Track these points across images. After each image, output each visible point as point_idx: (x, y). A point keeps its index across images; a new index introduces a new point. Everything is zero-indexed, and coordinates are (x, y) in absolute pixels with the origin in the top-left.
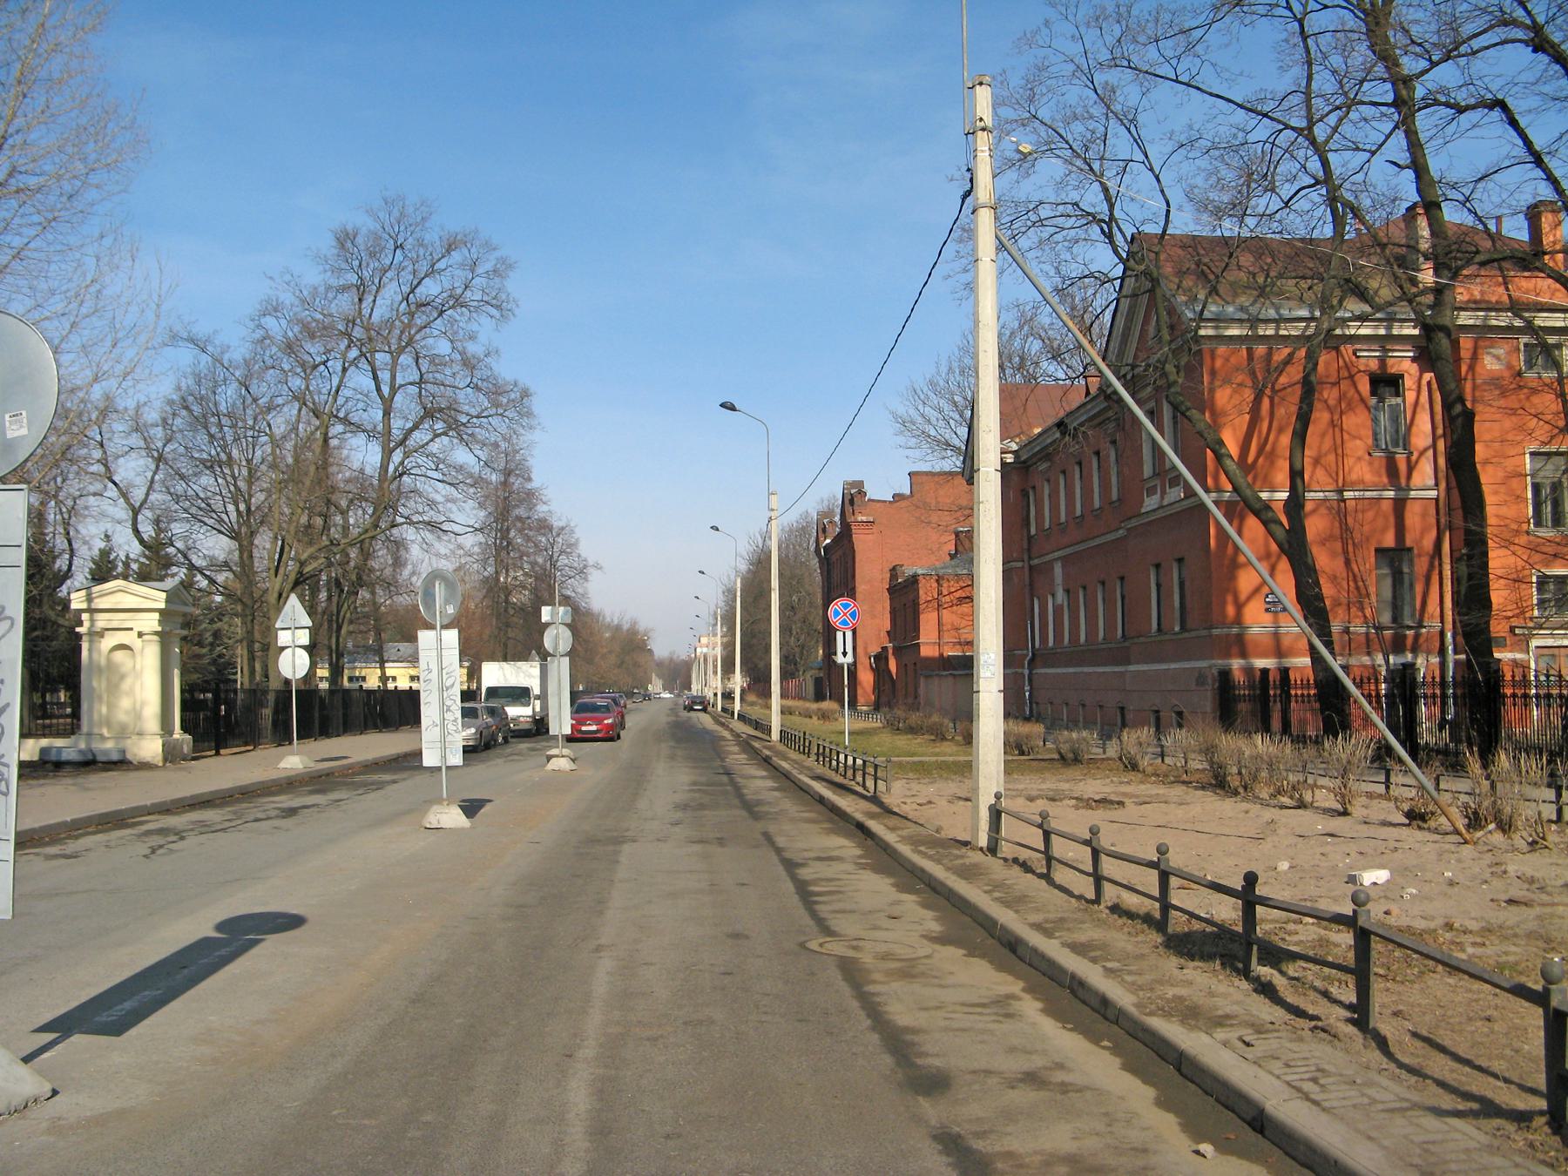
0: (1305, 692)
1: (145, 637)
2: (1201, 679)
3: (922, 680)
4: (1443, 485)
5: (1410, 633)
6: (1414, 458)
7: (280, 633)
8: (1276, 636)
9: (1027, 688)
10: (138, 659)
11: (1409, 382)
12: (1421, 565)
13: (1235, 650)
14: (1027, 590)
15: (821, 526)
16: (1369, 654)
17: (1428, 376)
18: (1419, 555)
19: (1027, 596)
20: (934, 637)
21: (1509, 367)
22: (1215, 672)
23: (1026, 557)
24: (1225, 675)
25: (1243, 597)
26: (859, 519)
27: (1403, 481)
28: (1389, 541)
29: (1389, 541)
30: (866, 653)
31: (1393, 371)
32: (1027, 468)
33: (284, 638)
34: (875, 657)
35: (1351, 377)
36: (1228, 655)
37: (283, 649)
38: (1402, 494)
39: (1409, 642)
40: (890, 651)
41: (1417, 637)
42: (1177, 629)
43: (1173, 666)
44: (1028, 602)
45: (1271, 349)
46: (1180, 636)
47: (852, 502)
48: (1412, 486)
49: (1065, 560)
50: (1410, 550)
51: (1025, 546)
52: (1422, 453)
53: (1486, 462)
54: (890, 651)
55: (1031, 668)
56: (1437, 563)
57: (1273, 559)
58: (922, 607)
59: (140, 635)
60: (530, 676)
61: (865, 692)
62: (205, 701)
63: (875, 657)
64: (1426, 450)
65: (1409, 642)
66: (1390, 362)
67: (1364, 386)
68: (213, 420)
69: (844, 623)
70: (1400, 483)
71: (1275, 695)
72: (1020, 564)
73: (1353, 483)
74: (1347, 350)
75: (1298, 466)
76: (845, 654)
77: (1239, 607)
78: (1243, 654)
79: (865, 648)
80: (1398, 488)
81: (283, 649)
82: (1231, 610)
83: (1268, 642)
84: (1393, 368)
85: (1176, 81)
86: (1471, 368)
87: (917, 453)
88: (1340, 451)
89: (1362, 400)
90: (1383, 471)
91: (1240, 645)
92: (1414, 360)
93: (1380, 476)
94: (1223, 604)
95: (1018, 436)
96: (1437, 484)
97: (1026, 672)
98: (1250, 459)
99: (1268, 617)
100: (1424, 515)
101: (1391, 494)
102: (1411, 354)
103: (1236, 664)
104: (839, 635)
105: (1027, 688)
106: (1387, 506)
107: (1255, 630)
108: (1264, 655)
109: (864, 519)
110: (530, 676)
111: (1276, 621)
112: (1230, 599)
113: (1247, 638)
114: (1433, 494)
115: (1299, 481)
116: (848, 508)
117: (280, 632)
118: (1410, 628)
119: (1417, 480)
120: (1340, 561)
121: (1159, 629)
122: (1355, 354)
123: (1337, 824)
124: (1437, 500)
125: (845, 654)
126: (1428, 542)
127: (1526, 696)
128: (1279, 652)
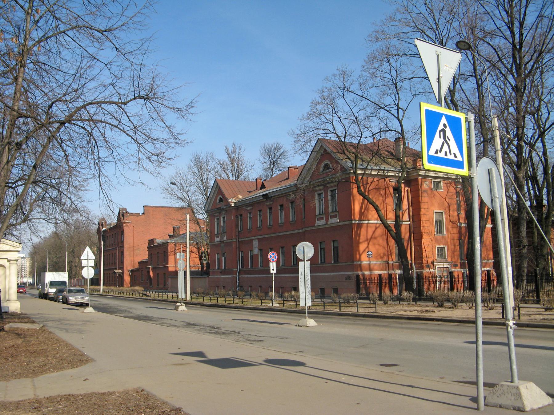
1: (11, 262)
2: (348, 278)
3: (170, 279)
4: (411, 220)
6: (403, 212)
7: (83, 261)
8: (369, 264)
9: (238, 282)
10: (7, 271)
13: (359, 269)
14: (238, 250)
15: (101, 223)
16: (393, 270)
17: (407, 188)
19: (238, 252)
20: (173, 264)
21: (429, 187)
22: (355, 275)
23: (237, 238)
24: (358, 276)
25: (361, 252)
26: (126, 221)
30: (127, 270)
32: (238, 208)
33: (84, 263)
34: (131, 271)
35: (388, 187)
36: (357, 271)
37: (84, 267)
40: (151, 269)
42: (333, 262)
43: (332, 274)
44: (238, 253)
45: (368, 178)
46: (321, 265)
47: (123, 215)
48: (403, 220)
49: (259, 240)
51: (237, 234)
52: (405, 211)
53: (424, 214)
54: (151, 269)
55: (239, 275)
56: (409, 243)
57: (369, 241)
58: (169, 254)
59: (9, 261)
60: (64, 277)
61: (127, 283)
63: (131, 271)
64: (406, 210)
67: (391, 190)
69: (273, 260)
72: (235, 240)
73: (389, 219)
74: (387, 179)
75: (398, 214)
76: (273, 270)
77: (360, 255)
78: (361, 270)
79: (127, 268)
81: (84, 267)
82: (358, 256)
83: (367, 266)
85: (363, 97)
86: (421, 187)
87: (168, 200)
88: (385, 209)
89: (391, 194)
91: (360, 267)
94: (356, 254)
95: (234, 197)
96: (409, 220)
97: (237, 276)
98: (363, 211)
99: (367, 259)
100: (406, 228)
103: (360, 273)
104: (271, 264)
105: (238, 282)
107: (364, 263)
108: (366, 270)
109: (128, 222)
110: (64, 277)
111: (369, 260)
112: (358, 253)
113: (362, 265)
114: (409, 223)
115: (398, 219)
116: (122, 218)
120: (385, 242)
121: (321, 262)
122: (389, 180)
124: (410, 225)
125: (273, 270)
127: (372, 282)
128: (370, 270)
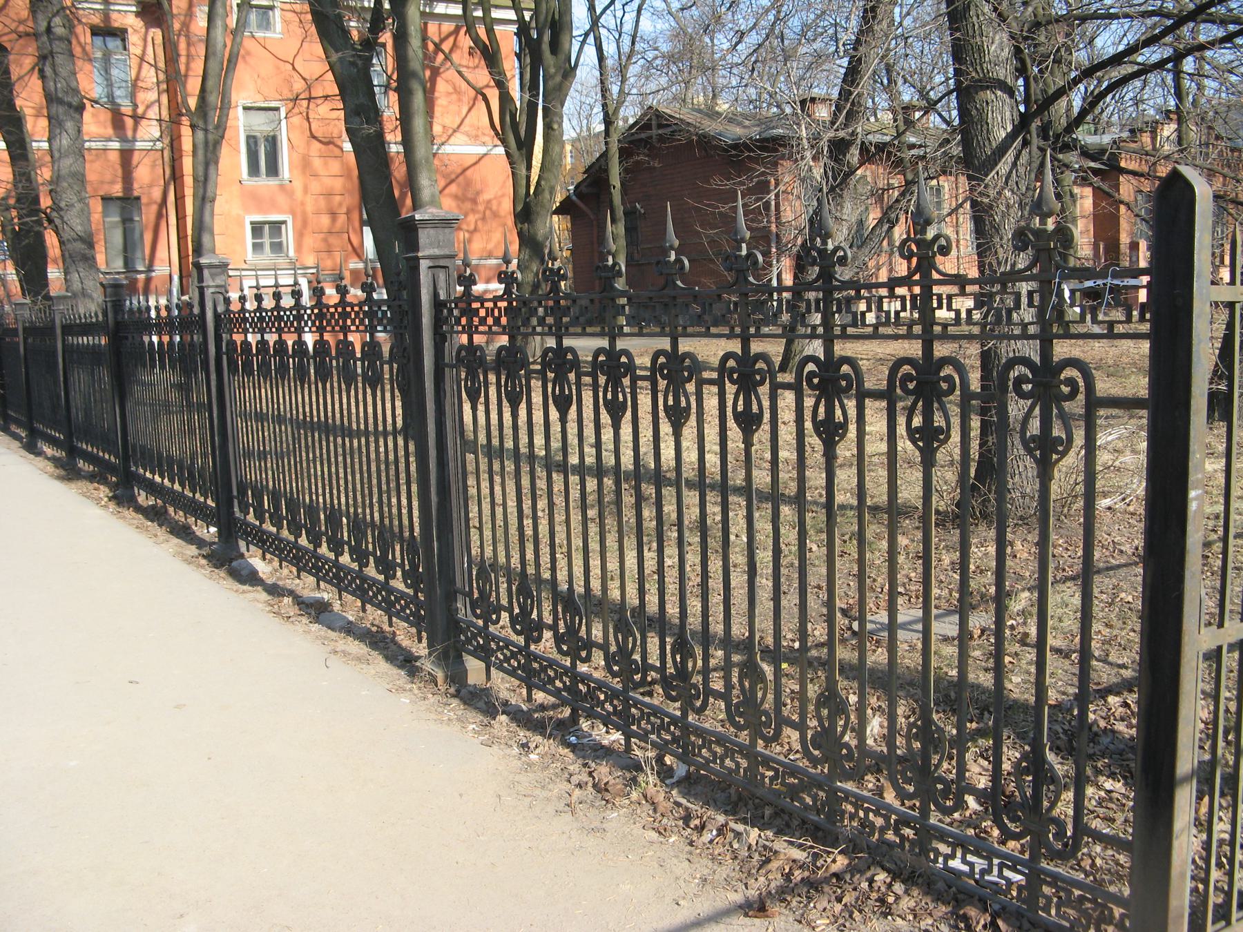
0: (271, 338)
5: (142, 277)
11: (134, 39)
12: (148, 215)
18: (148, 204)
27: (130, 134)
28: (117, 190)
29: (117, 190)
31: (116, 25)
38: (127, 146)
39: (141, 285)
41: (148, 280)
50: (138, 198)
62: (740, 249)
64: (152, 103)
65: (141, 285)
66: (114, 16)
68: (595, 667)
70: (125, 135)
71: (372, 349)
80: (123, 139)
84: (118, 21)
90: (109, 124)
92: (138, 14)
93: (105, 127)
101: (116, 145)
102: (134, 9)
106: (114, 157)
117: (1144, 393)
118: (141, 272)
119: (141, 133)
123: (1200, 680)
124: (162, 150)
126: (157, 193)
